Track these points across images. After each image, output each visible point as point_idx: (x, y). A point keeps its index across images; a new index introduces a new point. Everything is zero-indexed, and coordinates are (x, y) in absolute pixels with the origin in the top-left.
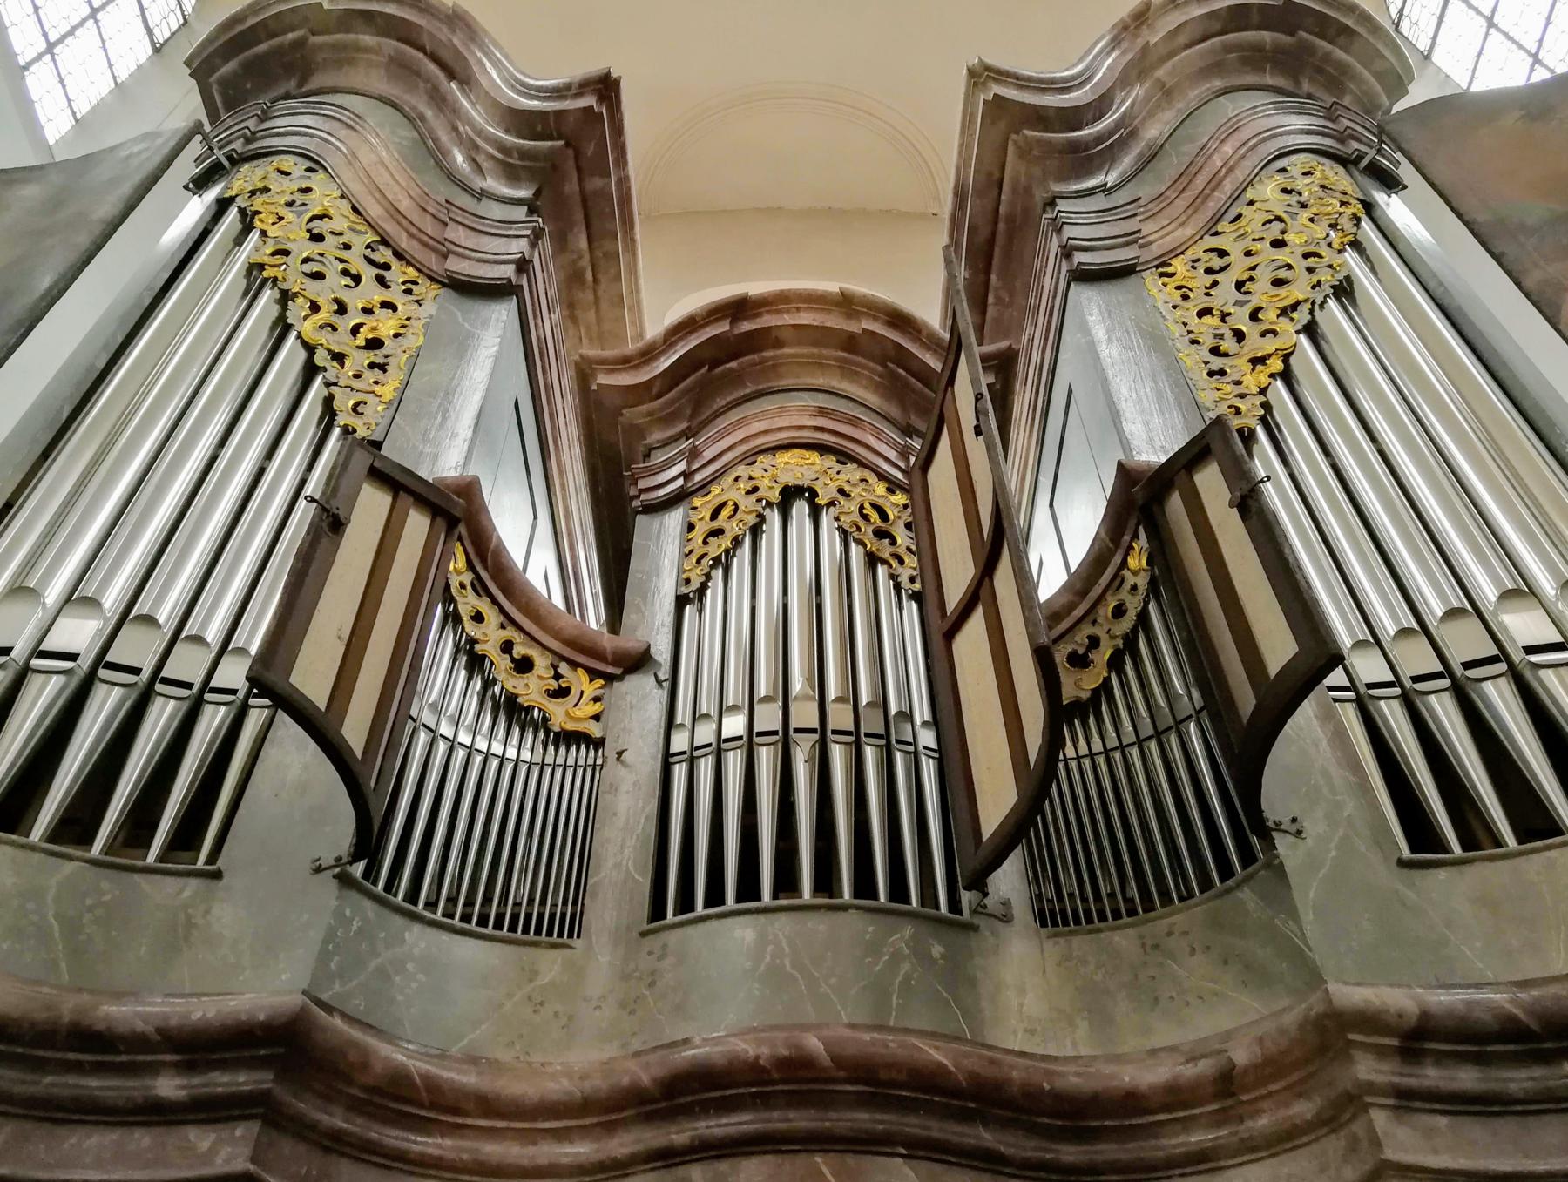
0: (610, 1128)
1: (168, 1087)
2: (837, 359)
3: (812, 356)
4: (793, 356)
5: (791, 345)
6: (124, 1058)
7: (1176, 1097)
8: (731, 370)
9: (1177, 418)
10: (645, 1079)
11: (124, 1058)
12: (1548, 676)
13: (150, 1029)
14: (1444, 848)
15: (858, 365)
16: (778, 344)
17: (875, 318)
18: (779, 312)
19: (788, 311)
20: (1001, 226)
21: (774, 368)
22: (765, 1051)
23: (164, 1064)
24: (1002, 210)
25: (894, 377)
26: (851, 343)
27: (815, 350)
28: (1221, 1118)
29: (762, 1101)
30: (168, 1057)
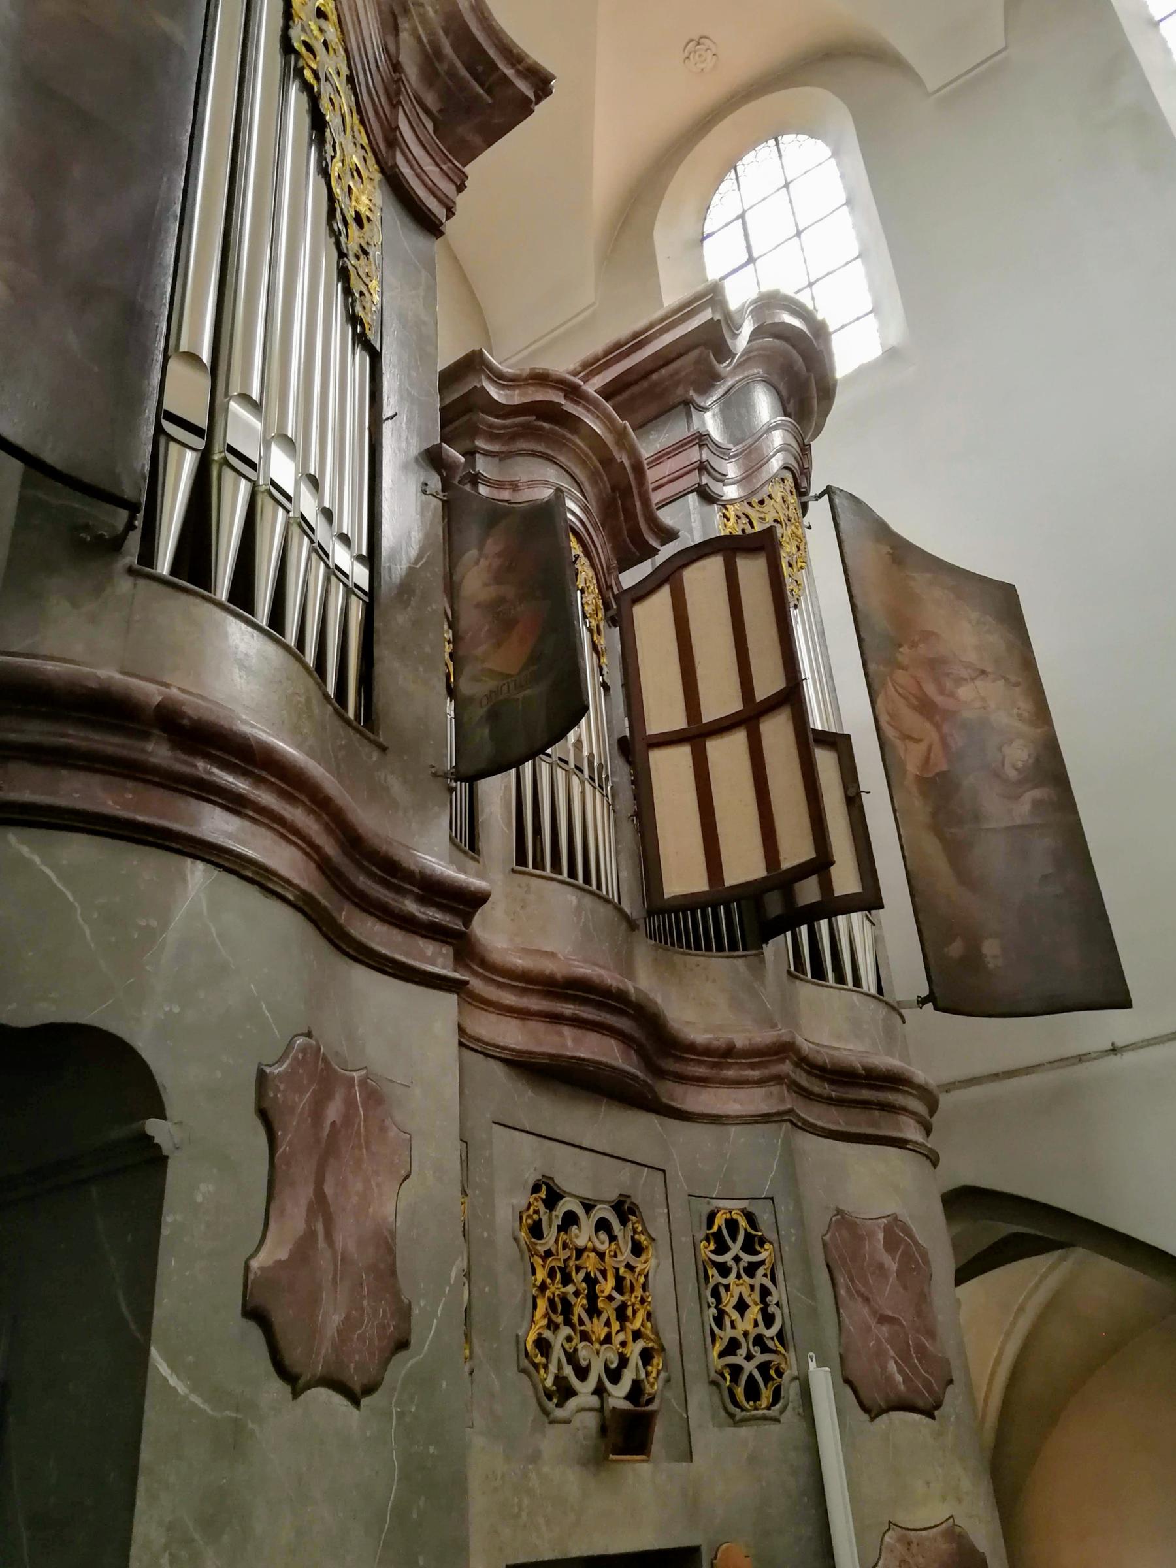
0: (524, 991)
1: (411, 907)
2: (595, 467)
3: (586, 455)
4: (579, 447)
5: (583, 439)
6: (395, 881)
7: (706, 1051)
8: (542, 429)
9: (414, 441)
10: (559, 976)
11: (395, 881)
12: (559, 770)
13: (417, 870)
14: (804, 973)
15: (602, 479)
16: (575, 431)
17: (629, 458)
18: (588, 410)
19: (593, 414)
20: (645, 384)
21: (561, 443)
22: (614, 984)
23: (411, 892)
24: (655, 377)
25: (614, 499)
26: (608, 461)
27: (591, 454)
28: (714, 1065)
29: (600, 1006)
30: (416, 890)
